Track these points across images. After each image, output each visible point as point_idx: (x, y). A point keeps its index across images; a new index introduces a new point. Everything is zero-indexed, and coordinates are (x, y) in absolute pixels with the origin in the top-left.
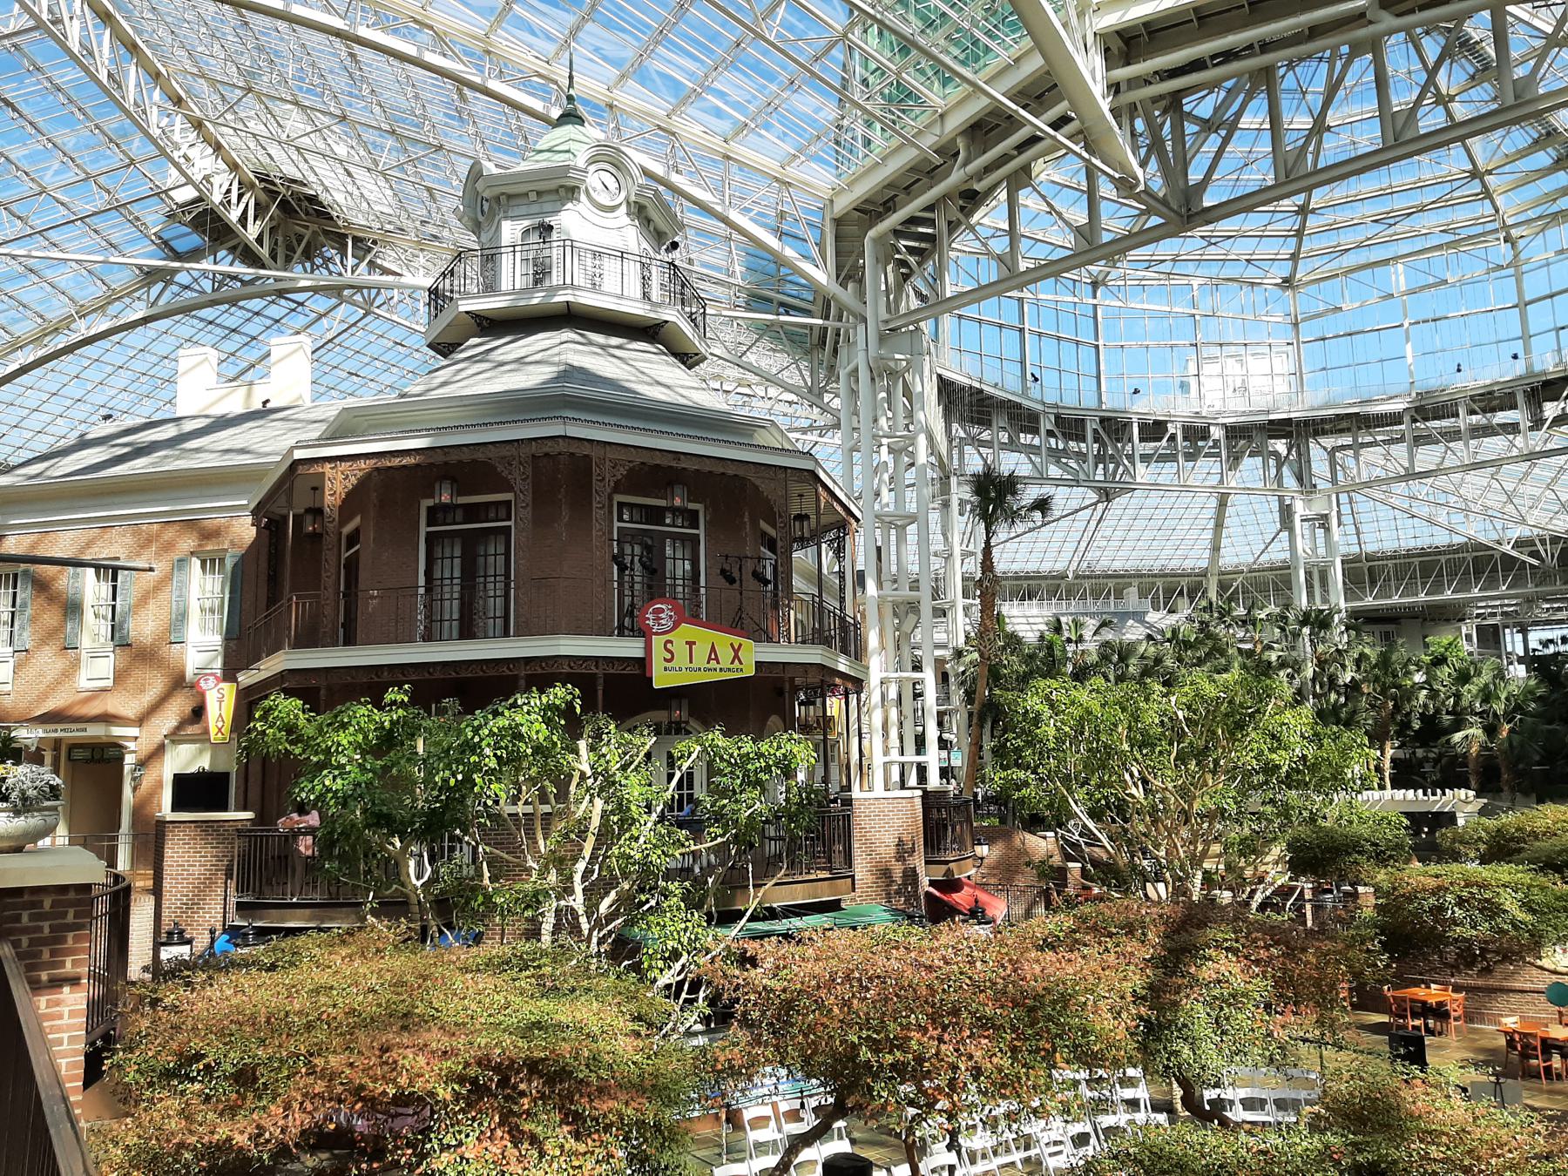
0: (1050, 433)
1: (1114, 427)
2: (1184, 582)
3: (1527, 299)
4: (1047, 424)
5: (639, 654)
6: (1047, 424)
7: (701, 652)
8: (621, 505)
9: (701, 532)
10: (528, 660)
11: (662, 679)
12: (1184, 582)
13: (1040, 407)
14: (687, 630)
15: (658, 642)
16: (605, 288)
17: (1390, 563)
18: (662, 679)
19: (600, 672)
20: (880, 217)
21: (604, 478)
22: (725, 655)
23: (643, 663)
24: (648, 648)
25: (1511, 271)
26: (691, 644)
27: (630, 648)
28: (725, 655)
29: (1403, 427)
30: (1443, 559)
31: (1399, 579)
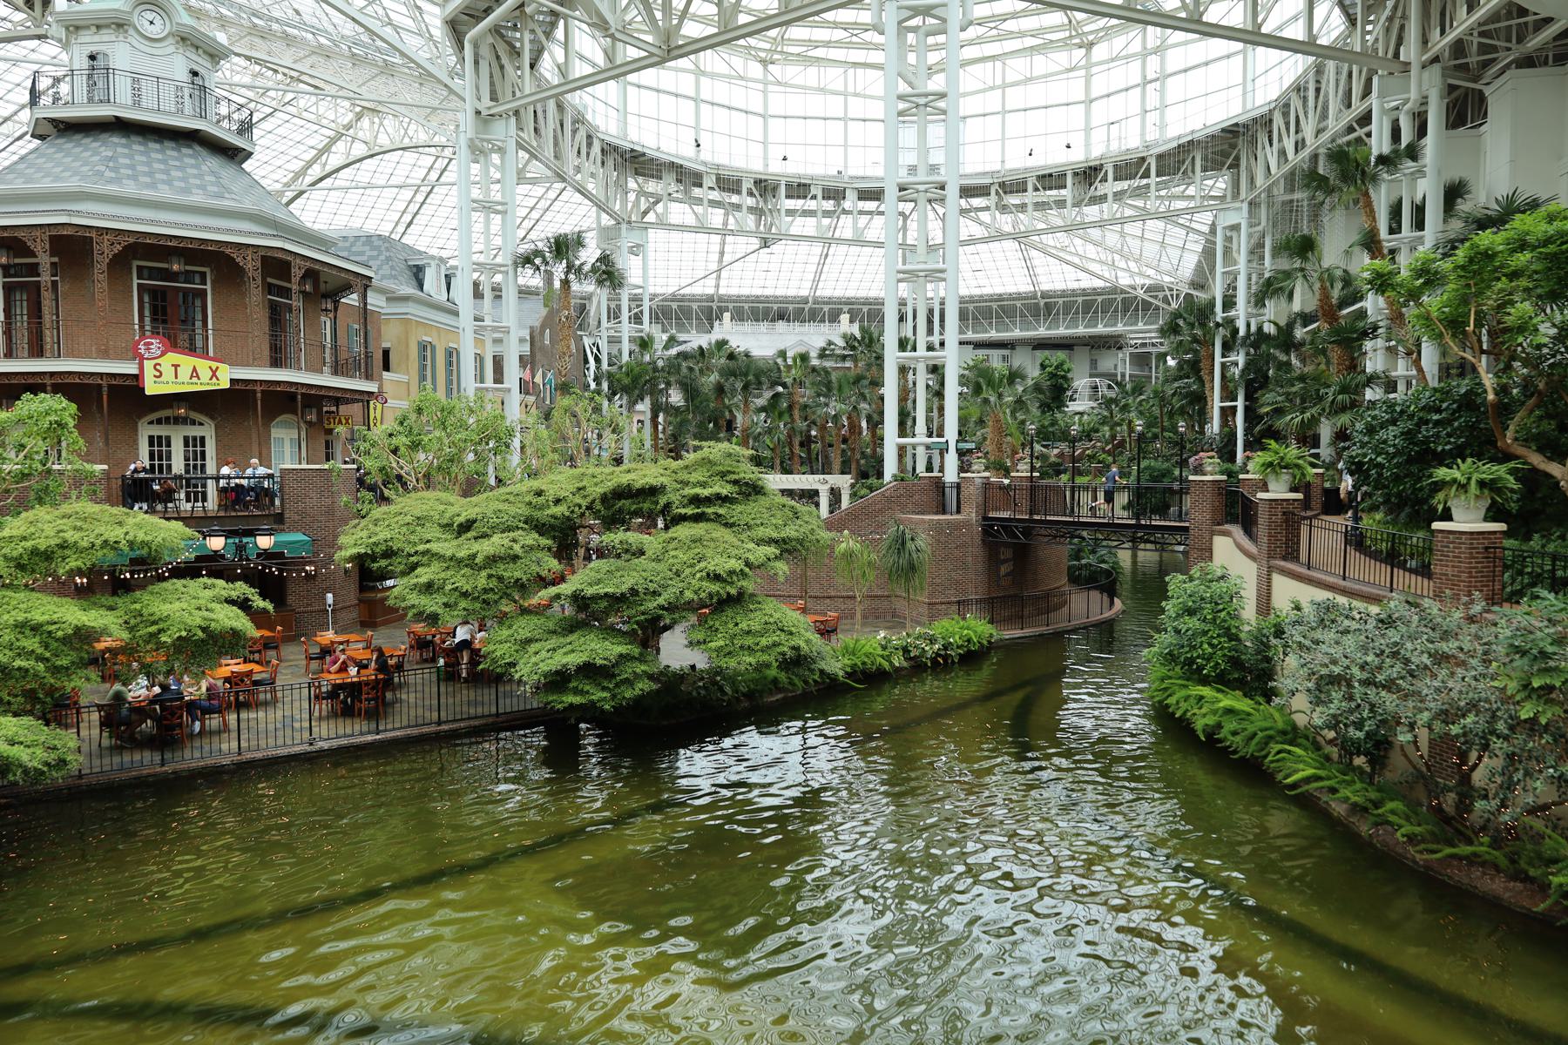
0: (711, 188)
1: (764, 187)
2: (826, 308)
3: (1093, 96)
4: (709, 181)
5: (135, 371)
6: (709, 181)
7: (184, 373)
8: (140, 268)
9: (208, 287)
10: (52, 374)
11: (151, 388)
12: (826, 308)
13: (702, 168)
14: (172, 357)
15: (148, 365)
16: (144, 104)
17: (1061, 301)
18: (151, 388)
19: (104, 383)
20: (479, 19)
21: (104, 252)
22: (205, 374)
23: (138, 377)
24: (141, 368)
25: (1083, 72)
26: (176, 366)
27: (130, 368)
28: (205, 374)
29: (1063, 192)
30: (1100, 299)
31: (1086, 312)
